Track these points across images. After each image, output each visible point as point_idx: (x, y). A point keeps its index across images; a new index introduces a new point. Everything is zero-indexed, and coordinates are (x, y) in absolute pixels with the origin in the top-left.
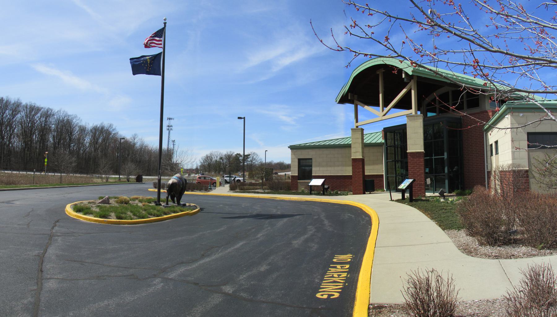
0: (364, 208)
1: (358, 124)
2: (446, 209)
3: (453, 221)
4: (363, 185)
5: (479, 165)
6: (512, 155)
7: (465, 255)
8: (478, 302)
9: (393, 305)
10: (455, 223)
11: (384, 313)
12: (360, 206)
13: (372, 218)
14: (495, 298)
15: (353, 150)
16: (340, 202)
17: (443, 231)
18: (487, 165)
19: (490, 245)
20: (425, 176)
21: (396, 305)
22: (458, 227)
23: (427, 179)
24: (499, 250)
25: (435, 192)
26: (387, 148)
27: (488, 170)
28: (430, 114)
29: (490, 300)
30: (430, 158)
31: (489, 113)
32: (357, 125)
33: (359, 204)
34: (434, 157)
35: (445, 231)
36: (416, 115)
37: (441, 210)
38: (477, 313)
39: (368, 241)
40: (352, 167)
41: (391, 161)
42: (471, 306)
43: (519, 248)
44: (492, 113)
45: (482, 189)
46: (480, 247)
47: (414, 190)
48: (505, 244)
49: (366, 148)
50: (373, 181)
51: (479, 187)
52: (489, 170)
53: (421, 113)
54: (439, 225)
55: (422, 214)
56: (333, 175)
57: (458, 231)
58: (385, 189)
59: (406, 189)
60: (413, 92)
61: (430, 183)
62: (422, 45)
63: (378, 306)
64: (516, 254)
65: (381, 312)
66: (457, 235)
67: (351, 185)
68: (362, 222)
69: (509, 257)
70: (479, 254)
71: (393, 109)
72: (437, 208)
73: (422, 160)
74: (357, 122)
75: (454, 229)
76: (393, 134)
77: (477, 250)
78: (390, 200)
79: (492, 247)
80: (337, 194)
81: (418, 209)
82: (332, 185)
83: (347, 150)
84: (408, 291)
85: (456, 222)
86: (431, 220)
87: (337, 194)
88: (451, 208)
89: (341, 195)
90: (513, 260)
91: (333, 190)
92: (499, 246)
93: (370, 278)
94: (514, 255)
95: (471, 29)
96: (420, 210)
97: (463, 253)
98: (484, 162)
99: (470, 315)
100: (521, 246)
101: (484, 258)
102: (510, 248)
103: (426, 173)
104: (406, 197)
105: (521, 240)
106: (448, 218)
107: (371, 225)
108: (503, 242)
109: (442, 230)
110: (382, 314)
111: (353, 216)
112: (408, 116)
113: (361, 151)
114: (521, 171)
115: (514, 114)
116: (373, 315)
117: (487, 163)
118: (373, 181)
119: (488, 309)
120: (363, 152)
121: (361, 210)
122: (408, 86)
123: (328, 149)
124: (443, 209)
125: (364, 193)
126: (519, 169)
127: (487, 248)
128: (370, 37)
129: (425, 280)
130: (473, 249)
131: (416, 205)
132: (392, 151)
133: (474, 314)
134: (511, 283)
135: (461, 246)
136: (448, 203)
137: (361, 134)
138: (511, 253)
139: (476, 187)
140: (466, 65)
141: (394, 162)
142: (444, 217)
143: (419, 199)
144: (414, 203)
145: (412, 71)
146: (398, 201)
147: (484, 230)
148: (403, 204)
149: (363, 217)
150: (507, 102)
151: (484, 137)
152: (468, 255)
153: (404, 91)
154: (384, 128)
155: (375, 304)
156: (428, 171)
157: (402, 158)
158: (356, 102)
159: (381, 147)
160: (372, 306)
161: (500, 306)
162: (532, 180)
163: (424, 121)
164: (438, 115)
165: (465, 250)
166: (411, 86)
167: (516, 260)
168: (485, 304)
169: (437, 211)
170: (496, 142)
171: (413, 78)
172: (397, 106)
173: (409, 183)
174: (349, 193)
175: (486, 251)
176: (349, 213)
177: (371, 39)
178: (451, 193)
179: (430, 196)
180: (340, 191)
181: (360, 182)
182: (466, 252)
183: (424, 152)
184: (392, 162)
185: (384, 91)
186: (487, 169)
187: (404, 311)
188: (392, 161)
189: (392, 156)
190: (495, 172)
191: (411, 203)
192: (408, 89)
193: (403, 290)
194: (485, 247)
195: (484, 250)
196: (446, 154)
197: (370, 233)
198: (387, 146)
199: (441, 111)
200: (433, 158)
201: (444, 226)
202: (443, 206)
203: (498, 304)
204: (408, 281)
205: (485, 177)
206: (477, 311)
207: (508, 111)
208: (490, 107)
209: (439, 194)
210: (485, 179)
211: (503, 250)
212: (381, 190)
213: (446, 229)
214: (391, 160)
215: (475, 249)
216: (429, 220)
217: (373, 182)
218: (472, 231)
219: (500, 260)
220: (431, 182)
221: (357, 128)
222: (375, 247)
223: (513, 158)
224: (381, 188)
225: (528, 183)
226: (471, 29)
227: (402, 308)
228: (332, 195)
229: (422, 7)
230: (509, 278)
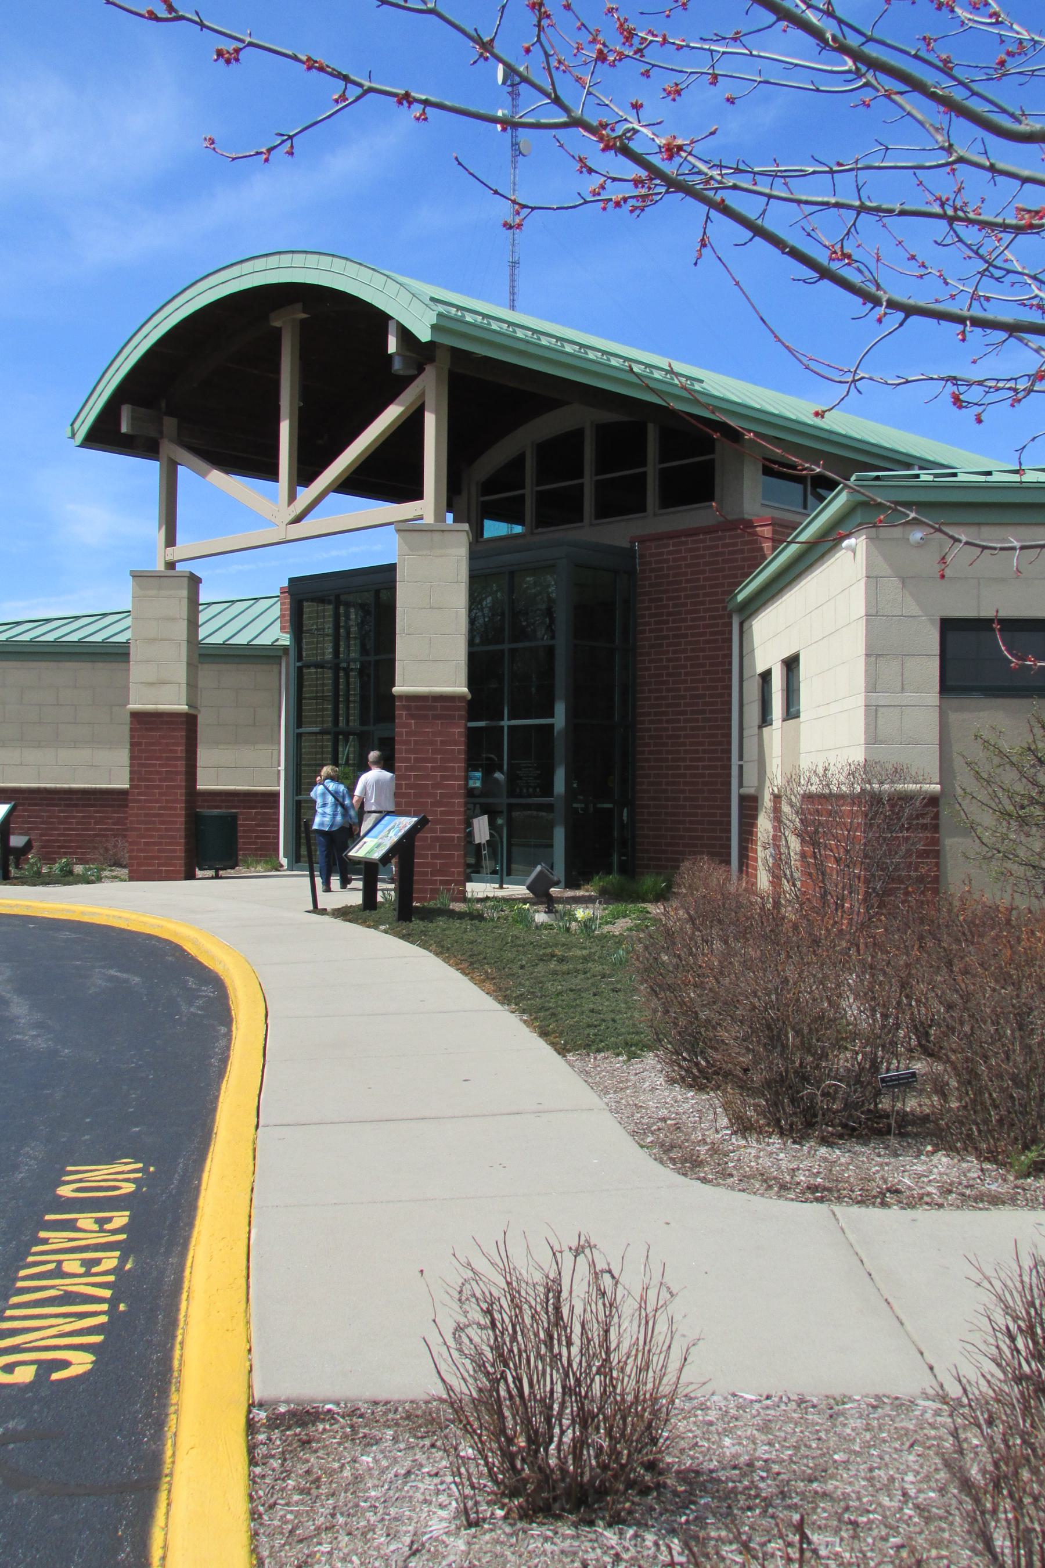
0: (194, 942)
1: (173, 554)
2: (562, 960)
3: (599, 1012)
4: (187, 837)
5: (704, 768)
6: (867, 724)
7: (667, 1175)
8: (757, 1406)
9: (363, 1408)
10: (610, 1024)
11: (325, 1447)
12: (176, 934)
13: (230, 991)
14: (837, 1392)
15: (138, 671)
16: (83, 913)
17: (559, 1057)
18: (741, 767)
19: (782, 1134)
20: (466, 803)
21: (376, 1403)
22: (627, 1044)
23: (475, 821)
24: (825, 1159)
25: (505, 878)
26: (300, 670)
27: (743, 791)
28: (494, 529)
29: (815, 1400)
30: (493, 724)
31: (758, 529)
32: (169, 558)
33: (171, 926)
34: (509, 719)
35: (570, 1057)
36: (440, 526)
37: (542, 960)
38: (766, 1461)
39: (217, 1097)
40: (132, 751)
41: (315, 734)
42: (729, 1422)
43: (917, 1157)
44: (774, 532)
45: (717, 875)
46: (738, 1141)
47: (421, 865)
48: (851, 1136)
49: (206, 666)
50: (234, 818)
51: (705, 864)
52: (752, 791)
53: (455, 521)
54: (540, 1027)
55: (458, 975)
56: (53, 785)
57: (629, 1060)
58: (284, 861)
59: (385, 859)
60: (430, 421)
61: (488, 838)
62: (641, 106)
63: (292, 1414)
64: (910, 1188)
65: (309, 1442)
66: (627, 1081)
67: (115, 836)
68: (184, 1008)
69: (875, 1197)
70: (735, 1172)
71: (333, 497)
72: (525, 953)
73: (458, 731)
74: (171, 541)
75: (607, 1048)
76: (330, 607)
77: (726, 1155)
78: (311, 907)
79: (794, 1142)
80: (71, 878)
81: (437, 954)
82: (42, 835)
83: (100, 672)
84: (458, 1340)
85: (614, 1021)
86: (498, 1006)
87: (67, 877)
88: (585, 952)
89: (89, 882)
90: (894, 1215)
91: (48, 858)
92: (825, 1141)
93: (245, 1273)
94: (897, 1191)
95: (845, 64)
96: (446, 960)
97: (662, 1162)
98: (729, 751)
99: (735, 1467)
100: (929, 1148)
101: (762, 1195)
102: (879, 1155)
103: (470, 793)
104: (380, 898)
105: (925, 1119)
106: (575, 1000)
107: (225, 1017)
108: (845, 1126)
109: (555, 1054)
110: (316, 1451)
111: (137, 979)
112: (405, 528)
113: (183, 679)
114: (907, 798)
115: (884, 532)
116: (273, 1456)
117: (741, 758)
118: (234, 818)
119: (814, 1445)
120: (192, 686)
121: (178, 950)
122: (409, 396)
123: (26, 664)
124: (553, 956)
125: (190, 876)
126: (900, 787)
127: (768, 1144)
128: (431, 5)
129: (542, 1289)
130: (703, 1149)
131: (425, 935)
132: (323, 685)
133: (750, 1464)
134: (902, 1324)
135: (647, 1130)
136: (568, 930)
137: (185, 602)
138: (885, 1181)
139: (687, 864)
140: (862, 209)
141: (328, 737)
142: (560, 994)
143: (439, 909)
144: (417, 924)
145: (433, 327)
146: (344, 913)
147: (756, 1062)
148: (369, 927)
149: (191, 983)
150: (853, 478)
151: (730, 640)
152: (685, 1175)
153: (391, 414)
154: (291, 580)
155: (277, 1402)
156: (478, 784)
157: (363, 721)
158: (169, 448)
159: (275, 668)
160: (263, 1415)
161: (868, 1436)
162: (953, 845)
163: (474, 556)
164: (532, 534)
165: (667, 1148)
166: (423, 394)
167: (910, 1213)
168: (795, 1415)
169: (522, 967)
170: (791, 664)
171: (431, 360)
172: (352, 484)
173: (400, 834)
174: (106, 873)
175: (766, 1162)
176: (111, 967)
177: (433, 18)
178: (577, 887)
179: (487, 898)
180: (82, 861)
181: (175, 823)
182: (673, 1160)
183: (469, 697)
184: (319, 737)
185: (300, 408)
186: (741, 785)
187: (422, 1437)
188: (323, 733)
189: (323, 710)
190: (777, 798)
191: (404, 927)
192: (412, 404)
193: (435, 1340)
194: (758, 1141)
195: (757, 1157)
196: (560, 709)
197: (225, 1060)
198: (299, 664)
199: (543, 520)
200: (502, 723)
201: (561, 1033)
202: (547, 945)
203: (859, 1423)
204: (460, 1292)
205: (729, 823)
206: (763, 1451)
207: (858, 518)
208: (763, 505)
209: (528, 888)
210: (729, 831)
211: (843, 1160)
212: (266, 862)
213: (575, 1048)
214: (317, 729)
215: (714, 1150)
216: (490, 1003)
217: (230, 823)
218: (697, 1064)
219: (837, 1208)
220: (491, 835)
221: (171, 573)
222: (257, 1126)
223: (873, 737)
224: (266, 853)
225: (937, 854)
226: (845, 64)
227: (408, 1418)
228: (47, 879)
229: (476, 30)
230: (890, 1300)
